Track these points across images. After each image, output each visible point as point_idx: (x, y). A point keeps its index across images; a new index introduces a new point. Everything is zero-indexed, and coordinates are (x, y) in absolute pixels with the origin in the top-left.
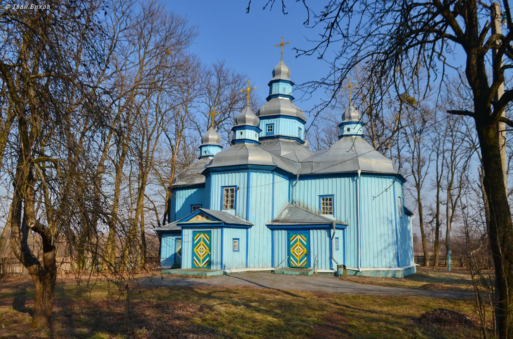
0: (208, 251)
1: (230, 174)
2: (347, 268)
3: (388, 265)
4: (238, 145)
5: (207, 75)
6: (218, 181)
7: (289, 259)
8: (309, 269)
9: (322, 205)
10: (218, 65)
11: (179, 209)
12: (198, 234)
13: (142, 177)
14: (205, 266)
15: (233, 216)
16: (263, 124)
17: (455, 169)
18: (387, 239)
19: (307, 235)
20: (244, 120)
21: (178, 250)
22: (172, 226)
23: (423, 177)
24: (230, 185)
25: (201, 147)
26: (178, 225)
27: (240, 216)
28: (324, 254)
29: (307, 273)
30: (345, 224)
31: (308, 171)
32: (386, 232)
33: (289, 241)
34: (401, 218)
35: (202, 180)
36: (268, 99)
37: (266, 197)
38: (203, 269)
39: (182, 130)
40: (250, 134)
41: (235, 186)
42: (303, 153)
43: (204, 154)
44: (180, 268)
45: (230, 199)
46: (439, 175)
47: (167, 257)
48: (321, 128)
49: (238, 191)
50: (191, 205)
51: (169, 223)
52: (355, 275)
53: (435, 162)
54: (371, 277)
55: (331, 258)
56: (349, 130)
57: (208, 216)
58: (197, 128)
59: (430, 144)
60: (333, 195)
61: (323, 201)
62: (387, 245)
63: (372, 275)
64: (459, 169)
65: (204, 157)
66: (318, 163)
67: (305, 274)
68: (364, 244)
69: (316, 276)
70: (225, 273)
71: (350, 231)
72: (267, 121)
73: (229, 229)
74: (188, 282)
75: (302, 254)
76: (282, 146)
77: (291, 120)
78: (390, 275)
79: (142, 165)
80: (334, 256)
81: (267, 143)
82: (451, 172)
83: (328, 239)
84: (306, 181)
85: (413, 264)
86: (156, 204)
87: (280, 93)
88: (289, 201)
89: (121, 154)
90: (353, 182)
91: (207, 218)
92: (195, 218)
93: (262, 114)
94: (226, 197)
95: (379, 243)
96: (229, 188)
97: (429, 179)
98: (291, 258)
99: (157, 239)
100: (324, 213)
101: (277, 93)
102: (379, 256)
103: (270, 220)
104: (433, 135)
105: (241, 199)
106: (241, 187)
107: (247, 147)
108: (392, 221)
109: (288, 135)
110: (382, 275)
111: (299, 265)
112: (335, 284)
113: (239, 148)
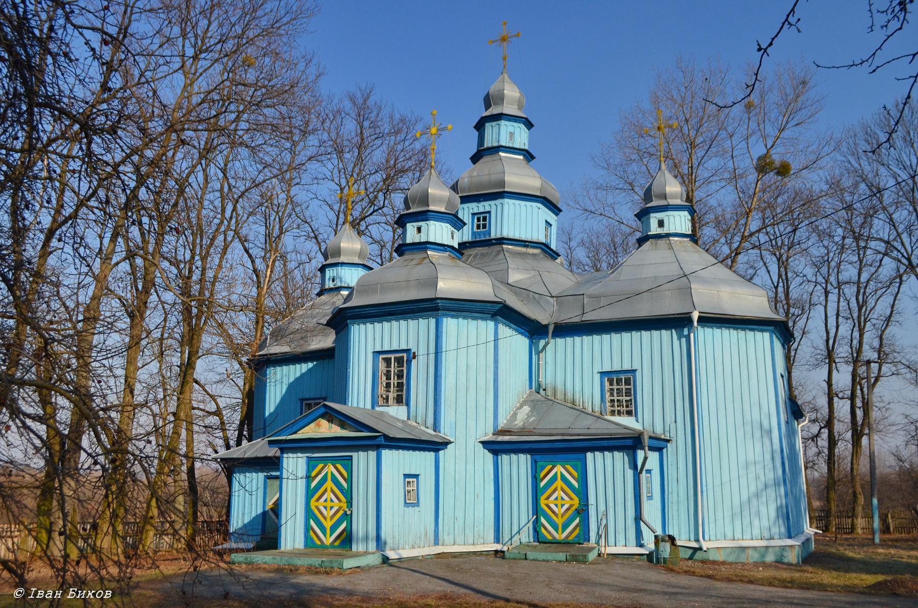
0: (345, 506)
1: (394, 323)
2: (679, 543)
3: (766, 535)
4: (412, 256)
5: (335, 117)
6: (366, 340)
7: (537, 521)
8: (585, 545)
9: (608, 394)
10: (359, 95)
11: (272, 410)
12: (321, 466)
13: (191, 339)
14: (337, 544)
15: (403, 422)
16: (466, 212)
17: (865, 322)
18: (762, 472)
19: (579, 464)
20: (424, 199)
21: (270, 504)
22: (257, 448)
23: (797, 340)
24: (395, 347)
25: (322, 269)
26: (270, 442)
27: (419, 420)
28: (618, 510)
29: (585, 557)
30: (663, 437)
31: (571, 316)
32: (759, 458)
33: (536, 480)
34: (787, 422)
35: (327, 341)
36: (475, 159)
37: (478, 377)
38: (332, 551)
39: (279, 237)
40: (438, 232)
41: (407, 351)
42: (559, 277)
43: (329, 284)
44: (276, 548)
45: (394, 381)
46: (832, 335)
47: (246, 521)
48: (578, 239)
49: (414, 362)
50: (302, 400)
51: (250, 440)
52: (691, 558)
53: (821, 309)
54: (731, 564)
55: (639, 518)
56: (661, 224)
57: (344, 420)
58: (312, 235)
59: (809, 272)
60: (633, 371)
61: (611, 384)
62: (761, 486)
63: (731, 559)
64: (874, 321)
65: (331, 290)
66: (597, 297)
67: (580, 559)
68: (710, 486)
69: (606, 562)
70: (386, 560)
71: (678, 454)
72: (475, 207)
73: (395, 452)
74: (296, 586)
75: (568, 509)
76: (512, 263)
77: (529, 204)
78: (770, 558)
79: (190, 312)
80: (646, 515)
81: (476, 255)
82: (856, 328)
83: (630, 473)
84: (569, 340)
85: (809, 530)
86: (222, 403)
87: (503, 143)
88: (531, 387)
89: (140, 287)
90: (679, 339)
91: (343, 426)
92: (312, 425)
93: (463, 190)
94: (384, 378)
95: (743, 481)
96: (392, 356)
97: (810, 344)
98: (543, 520)
99: (223, 479)
100: (613, 413)
101: (495, 144)
102: (746, 513)
103: (491, 430)
104: (817, 251)
105: (420, 380)
106: (422, 351)
107: (434, 260)
108: (770, 431)
109: (523, 238)
110: (754, 557)
111: (561, 536)
112: (663, 583)
113: (414, 262)
